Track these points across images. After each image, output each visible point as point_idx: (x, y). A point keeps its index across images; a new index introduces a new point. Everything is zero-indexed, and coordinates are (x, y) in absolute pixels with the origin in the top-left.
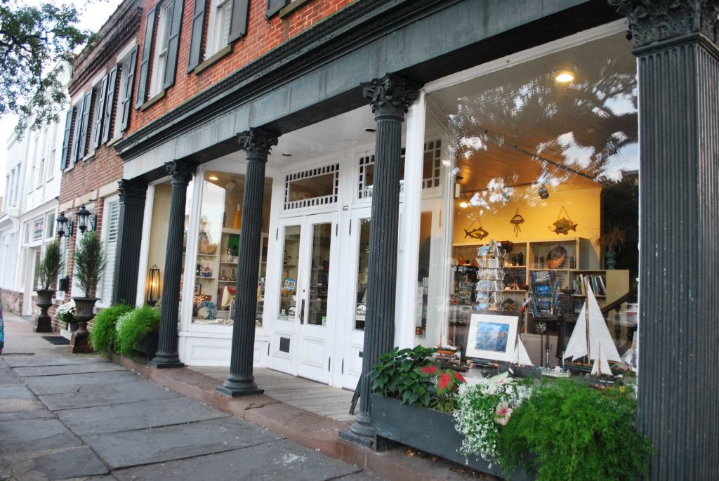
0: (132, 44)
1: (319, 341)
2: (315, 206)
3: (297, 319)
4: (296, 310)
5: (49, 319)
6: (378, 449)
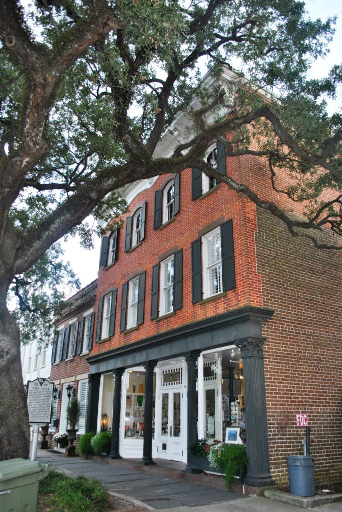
0: (91, 311)
1: (178, 444)
2: (174, 385)
3: (169, 435)
4: (169, 430)
5: (47, 442)
6: (192, 473)
